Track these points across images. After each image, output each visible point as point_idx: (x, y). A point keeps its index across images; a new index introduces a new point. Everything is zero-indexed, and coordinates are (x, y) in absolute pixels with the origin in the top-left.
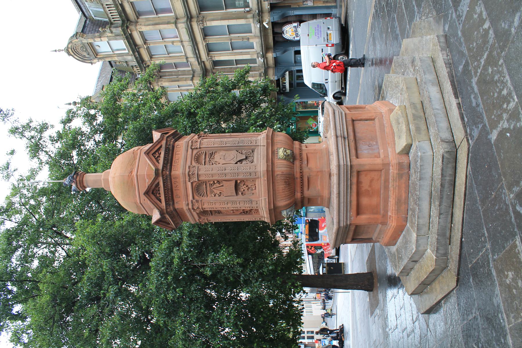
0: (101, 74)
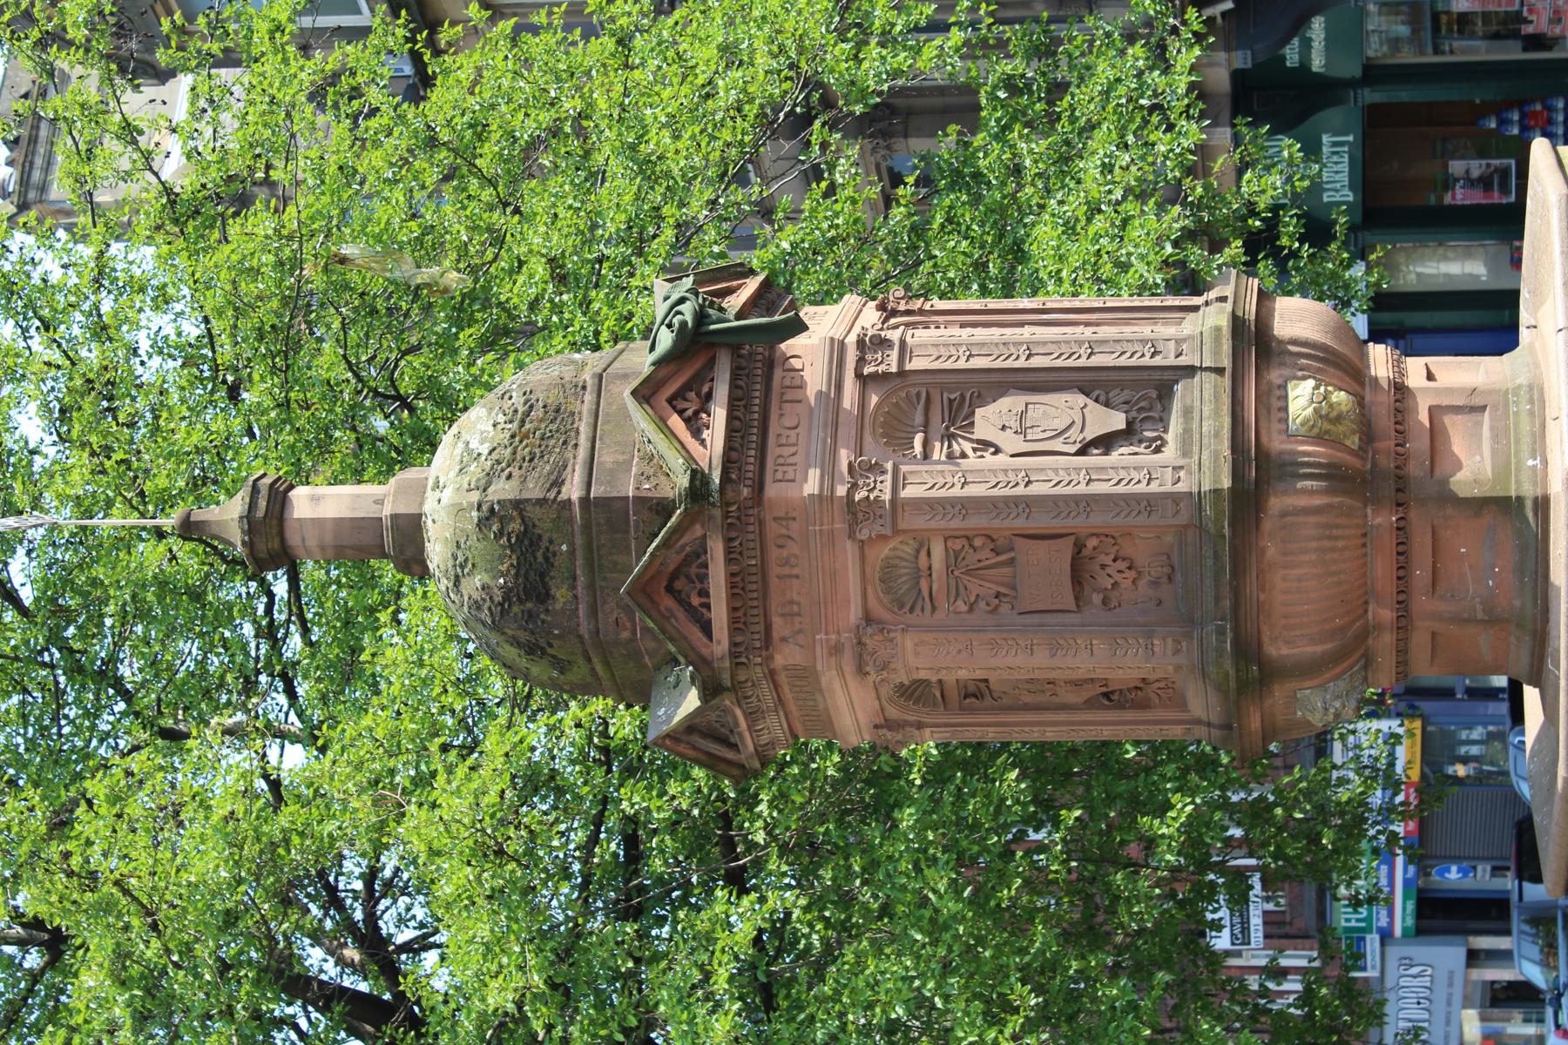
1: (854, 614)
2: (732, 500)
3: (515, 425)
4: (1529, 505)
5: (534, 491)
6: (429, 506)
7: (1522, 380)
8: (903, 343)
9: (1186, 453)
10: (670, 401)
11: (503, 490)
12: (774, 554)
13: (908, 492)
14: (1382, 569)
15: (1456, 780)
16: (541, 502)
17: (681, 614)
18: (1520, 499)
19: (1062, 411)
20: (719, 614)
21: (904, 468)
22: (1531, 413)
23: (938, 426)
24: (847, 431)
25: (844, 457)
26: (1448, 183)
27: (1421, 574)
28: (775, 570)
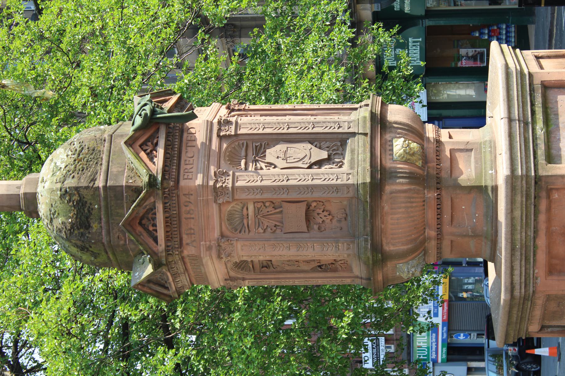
0: (207, 277)
1: (217, 234)
2: (166, 186)
3: (76, 156)
4: (490, 189)
5: (84, 183)
6: (40, 189)
7: (487, 138)
8: (237, 123)
9: (352, 168)
10: (140, 146)
11: (71, 183)
12: (183, 209)
13: (239, 184)
14: (431, 215)
15: (463, 299)
16: (87, 188)
17: (145, 234)
18: (486, 187)
19: (301, 150)
20: (161, 234)
21: (237, 174)
22: (491, 152)
23: (251, 157)
24: (214, 159)
25: (213, 169)
26: (459, 58)
27: (446, 217)
28: (184, 216)
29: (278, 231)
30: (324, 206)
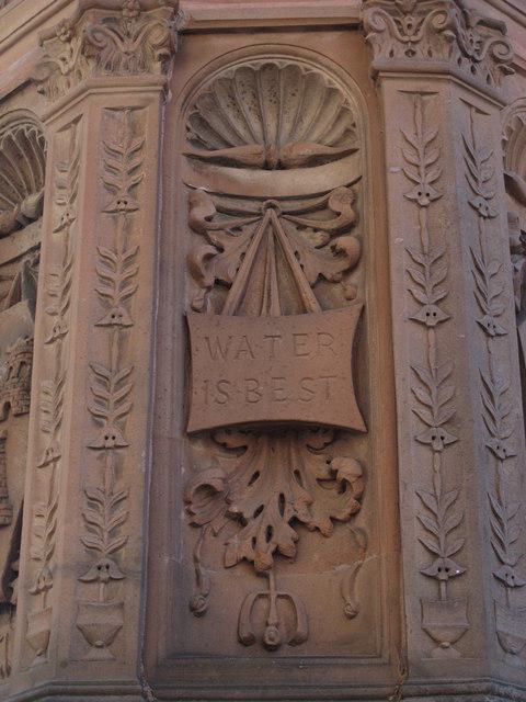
29: (193, 293)
30: (325, 525)
